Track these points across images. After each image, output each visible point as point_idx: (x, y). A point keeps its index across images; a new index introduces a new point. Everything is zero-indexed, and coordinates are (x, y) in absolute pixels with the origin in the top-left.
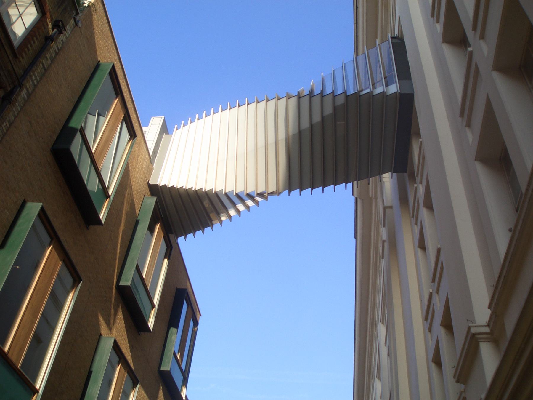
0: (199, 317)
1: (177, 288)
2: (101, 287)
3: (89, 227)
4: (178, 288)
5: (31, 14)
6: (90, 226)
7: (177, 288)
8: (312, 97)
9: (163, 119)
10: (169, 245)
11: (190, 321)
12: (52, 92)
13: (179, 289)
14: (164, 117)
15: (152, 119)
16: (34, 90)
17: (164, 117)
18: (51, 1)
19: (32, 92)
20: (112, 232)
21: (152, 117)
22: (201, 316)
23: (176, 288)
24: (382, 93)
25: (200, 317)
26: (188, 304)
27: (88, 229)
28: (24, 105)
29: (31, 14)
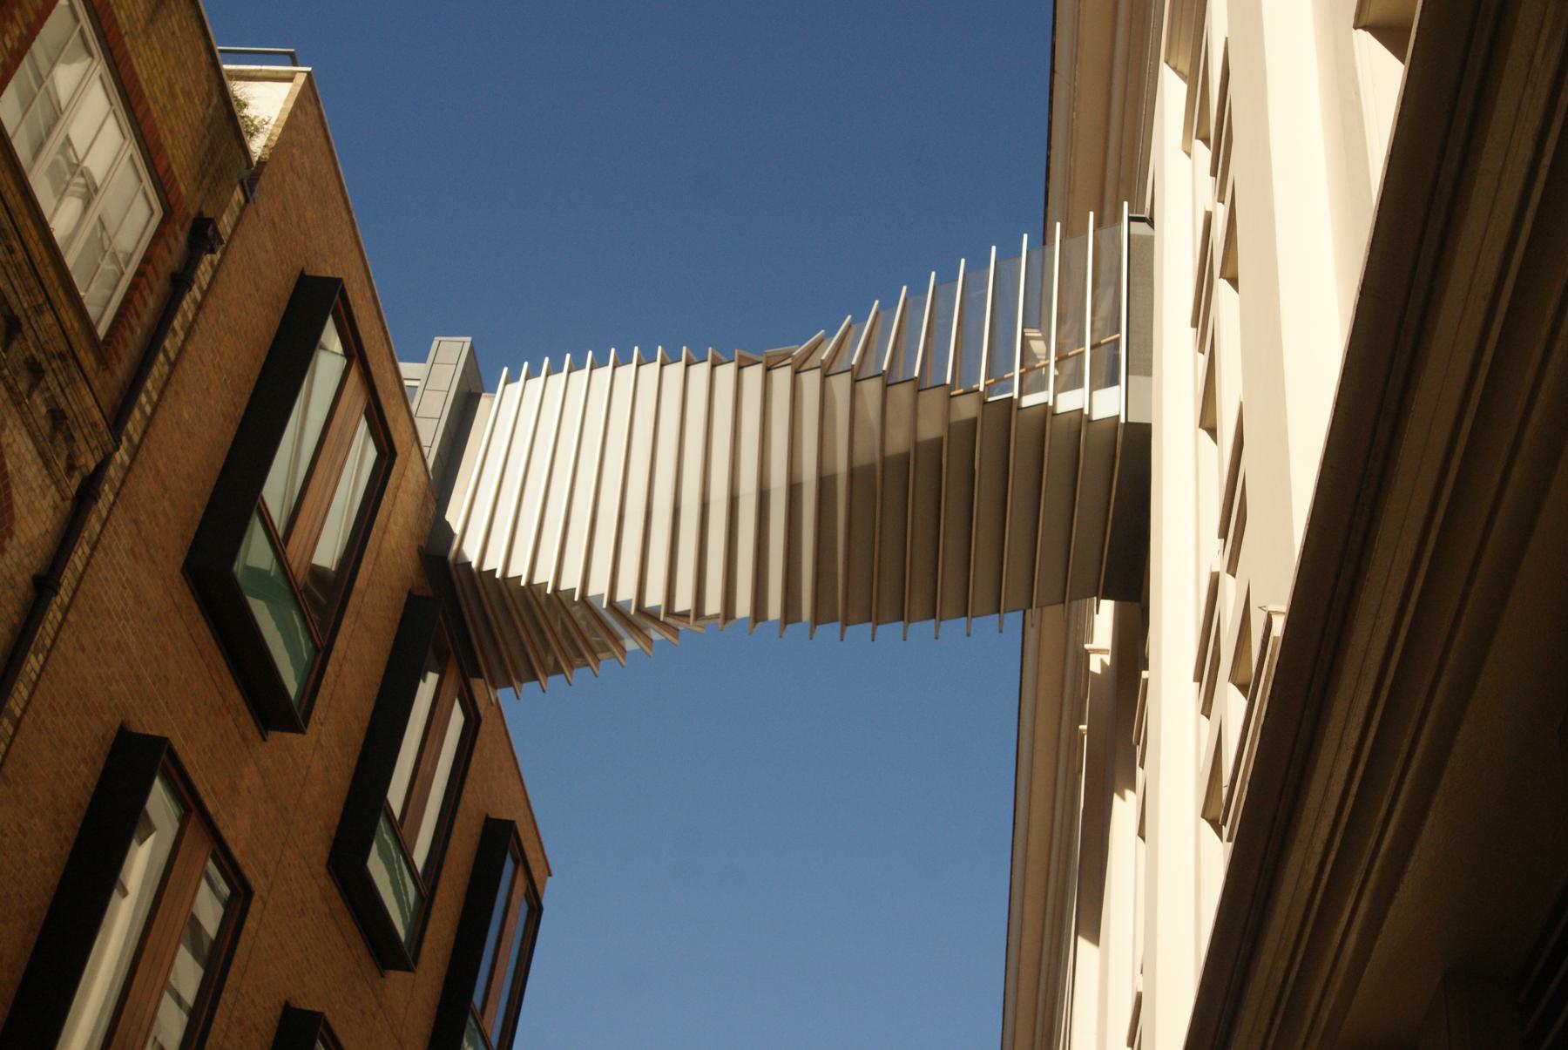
0: (544, 882)
1: (302, 272)
2: (291, 880)
3: (267, 735)
4: (307, 273)
5: (79, 89)
6: (269, 732)
7: (302, 272)
8: (922, 390)
9: (467, 346)
10: (387, 449)
11: (505, 858)
12: (187, 417)
13: (493, 820)
14: (469, 339)
15: (435, 344)
16: (145, 432)
17: (469, 339)
18: (130, 1)
19: (142, 440)
20: (322, 724)
21: (436, 338)
22: (550, 875)
23: (484, 817)
24: (1113, 344)
25: (549, 878)
26: (516, 862)
27: (265, 740)
28: (123, 483)
29: (79, 89)
